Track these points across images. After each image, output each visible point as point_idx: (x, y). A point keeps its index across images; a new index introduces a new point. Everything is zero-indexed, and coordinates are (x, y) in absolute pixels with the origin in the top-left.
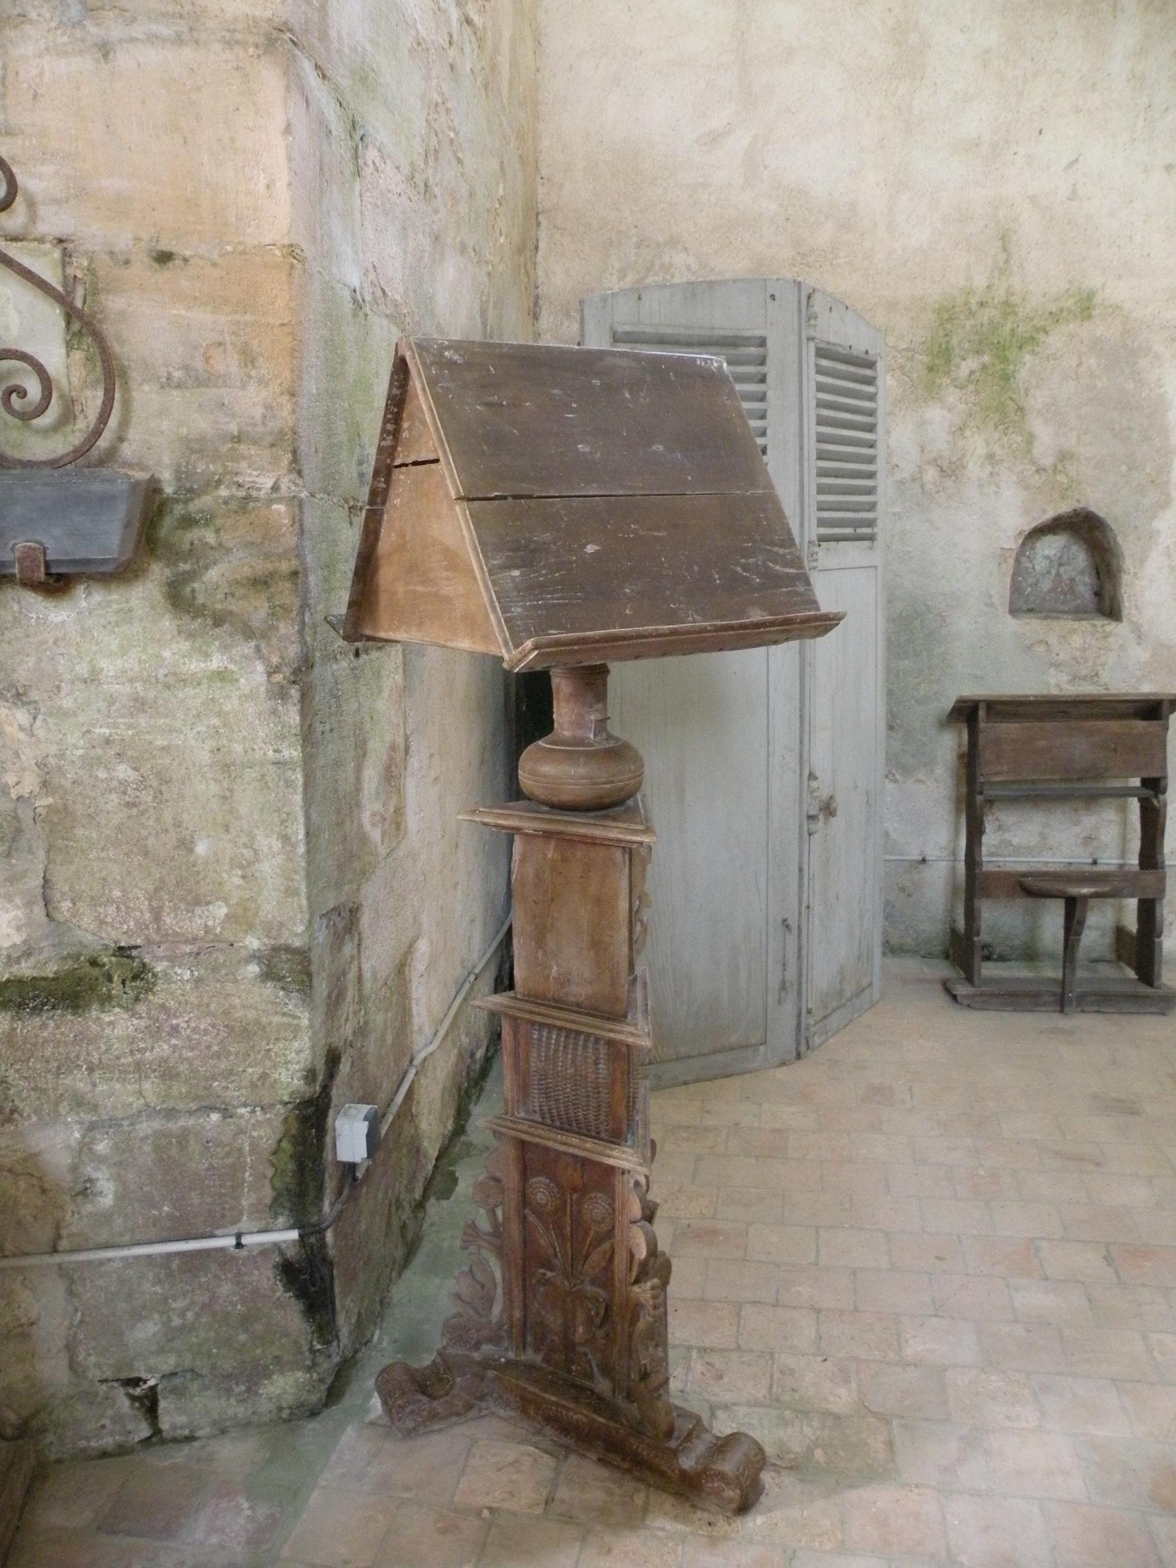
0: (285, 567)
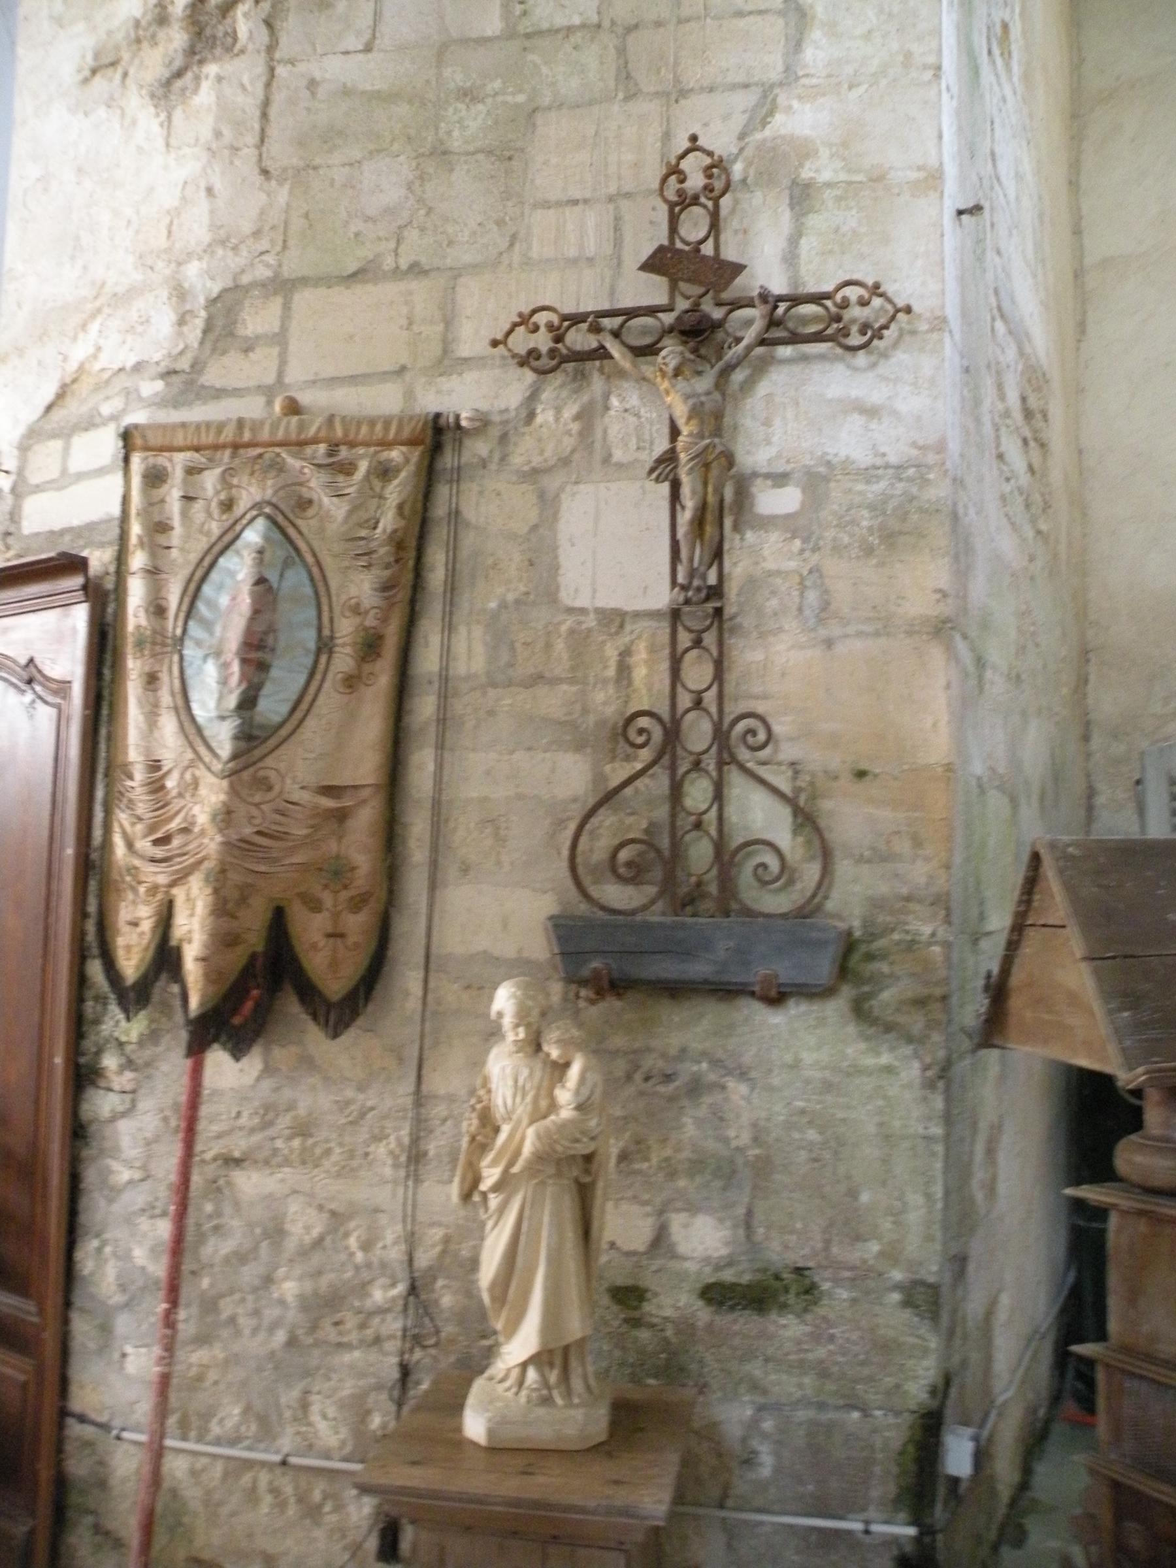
0: (938, 992)
